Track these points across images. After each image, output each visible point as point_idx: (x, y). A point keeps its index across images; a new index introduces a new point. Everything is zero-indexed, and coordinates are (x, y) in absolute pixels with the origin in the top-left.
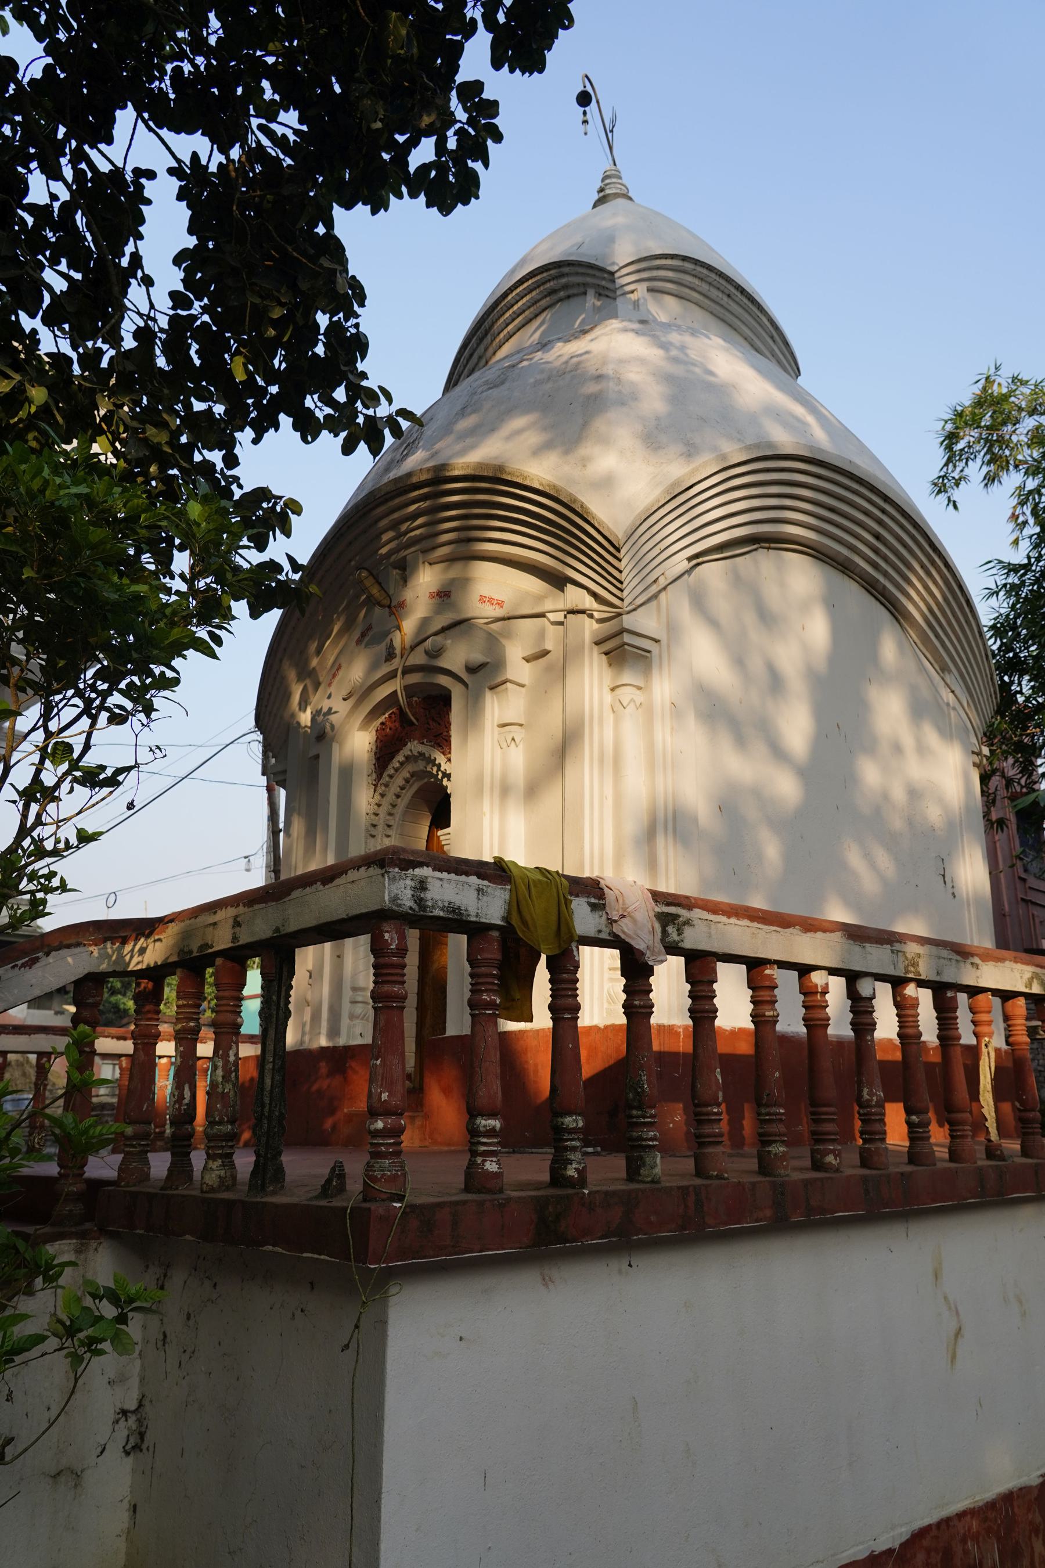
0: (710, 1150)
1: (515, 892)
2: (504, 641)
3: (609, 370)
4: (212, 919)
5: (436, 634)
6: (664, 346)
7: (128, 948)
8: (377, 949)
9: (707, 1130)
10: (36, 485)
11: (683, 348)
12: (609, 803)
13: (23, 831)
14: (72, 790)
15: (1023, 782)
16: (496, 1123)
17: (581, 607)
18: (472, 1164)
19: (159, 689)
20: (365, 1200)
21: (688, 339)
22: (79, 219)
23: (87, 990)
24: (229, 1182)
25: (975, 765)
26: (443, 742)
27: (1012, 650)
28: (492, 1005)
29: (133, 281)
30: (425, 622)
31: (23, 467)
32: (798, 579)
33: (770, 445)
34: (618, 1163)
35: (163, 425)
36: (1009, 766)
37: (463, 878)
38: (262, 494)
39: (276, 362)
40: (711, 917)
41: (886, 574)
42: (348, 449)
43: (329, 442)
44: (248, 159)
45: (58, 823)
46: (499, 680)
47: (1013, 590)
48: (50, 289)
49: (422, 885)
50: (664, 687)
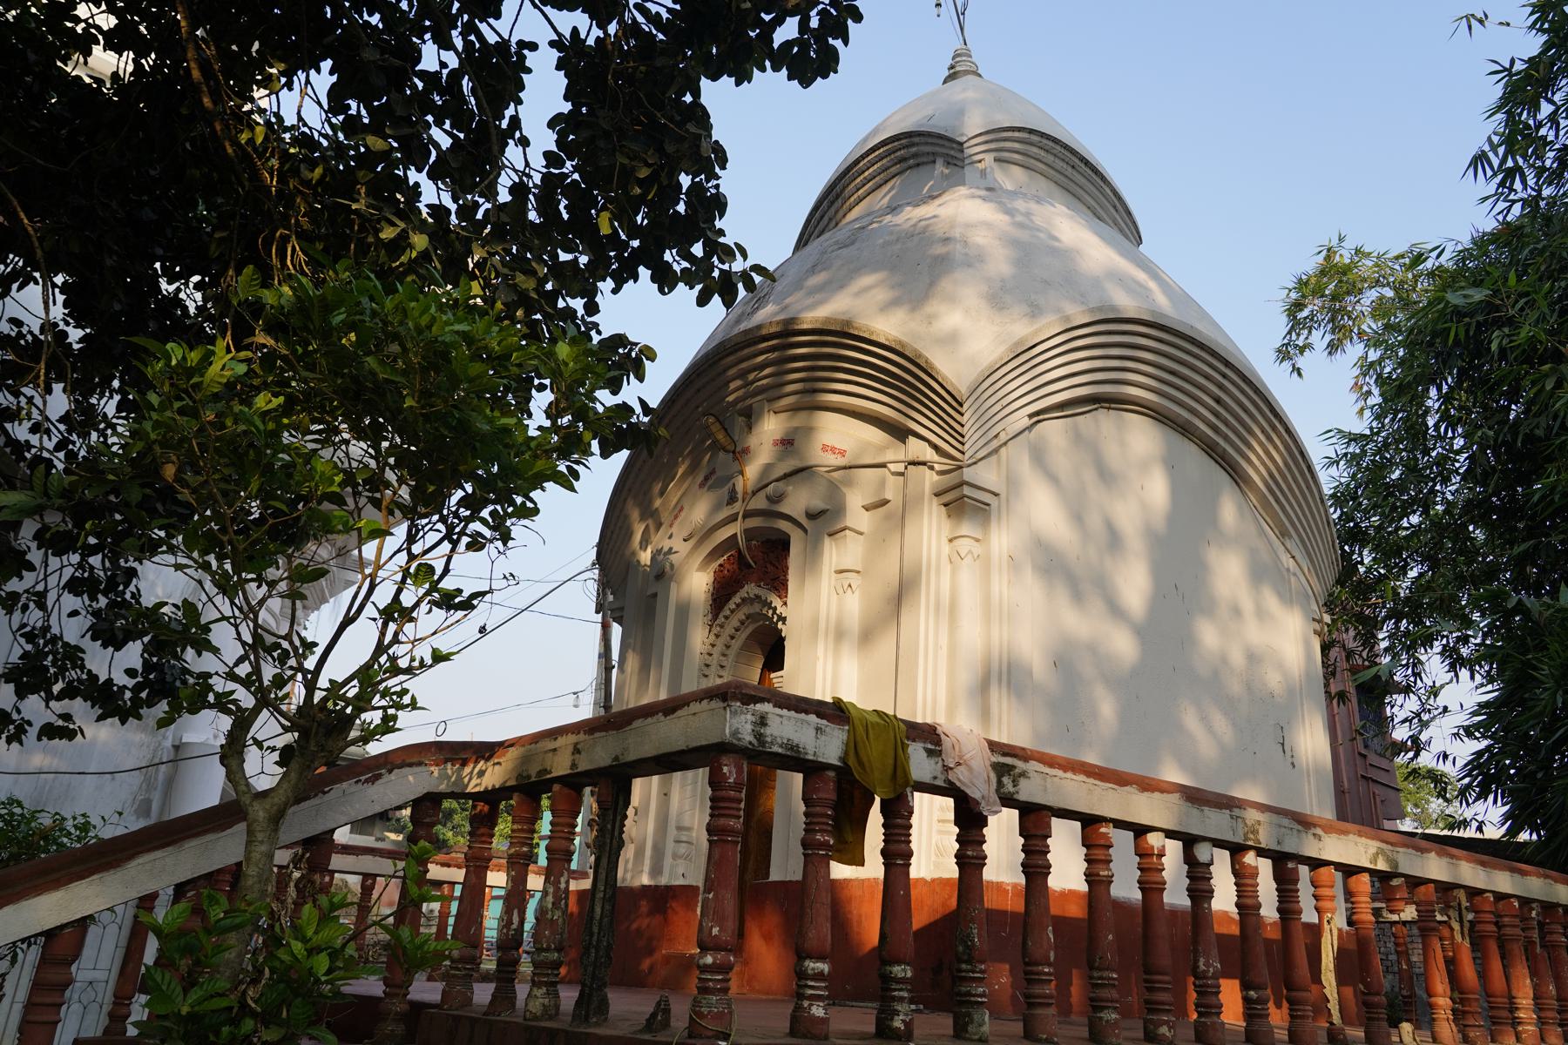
0: (1039, 1011)
1: (853, 733)
2: (844, 490)
3: (957, 233)
4: (551, 745)
5: (777, 480)
6: (1009, 212)
7: (467, 770)
8: (715, 782)
9: (1037, 990)
10: (424, 321)
11: (1028, 214)
12: (944, 652)
13: (380, 649)
14: (430, 611)
15: (1365, 654)
16: (824, 967)
17: (921, 459)
18: (798, 1008)
19: (519, 518)
20: (690, 1037)
21: (1033, 206)
22: (466, 84)
23: (427, 806)
24: (552, 1012)
25: (1315, 632)
26: (780, 586)
27: (1352, 520)
28: (825, 845)
29: (511, 142)
30: (768, 468)
31: (413, 304)
32: (1137, 440)
33: (1113, 308)
34: (945, 1022)
35: (534, 273)
36: (1349, 638)
37: (803, 716)
38: (619, 340)
39: (639, 219)
40: (1047, 770)
41: (1226, 438)
42: (703, 301)
43: (685, 294)
44: (624, 34)
45: (415, 642)
46: (839, 527)
47: (1353, 459)
48: (437, 146)
49: (762, 721)
50: (1002, 539)
